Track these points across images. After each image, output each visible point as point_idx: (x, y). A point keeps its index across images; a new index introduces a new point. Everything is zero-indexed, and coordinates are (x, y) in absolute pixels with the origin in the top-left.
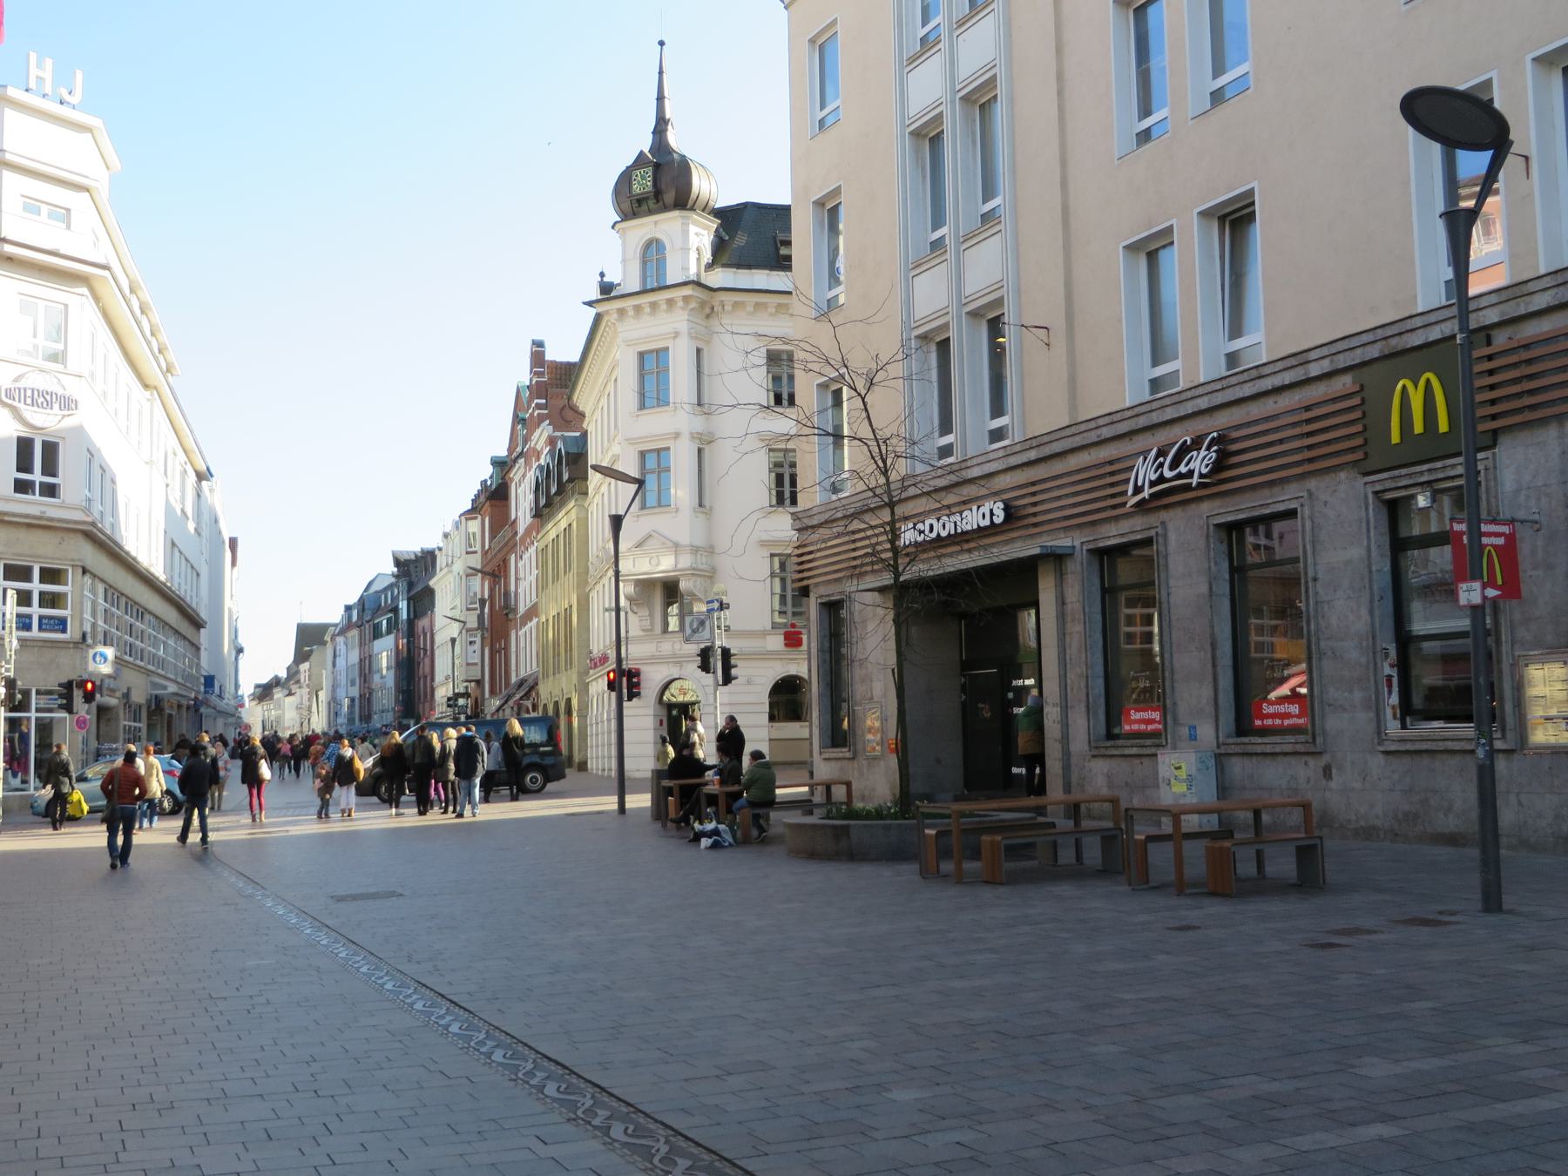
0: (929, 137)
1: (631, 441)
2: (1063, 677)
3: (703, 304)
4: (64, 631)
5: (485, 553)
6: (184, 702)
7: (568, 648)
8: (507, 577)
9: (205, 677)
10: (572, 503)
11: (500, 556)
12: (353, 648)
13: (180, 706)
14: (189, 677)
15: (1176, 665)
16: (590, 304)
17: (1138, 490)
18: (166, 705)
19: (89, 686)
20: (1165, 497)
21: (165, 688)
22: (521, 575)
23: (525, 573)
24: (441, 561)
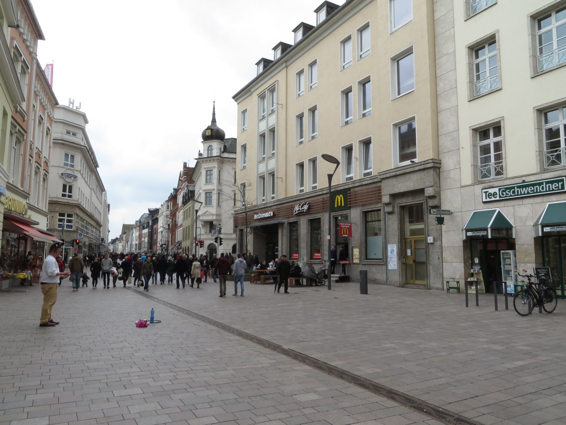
0: (263, 136)
1: (204, 190)
2: (282, 247)
3: (221, 161)
4: (72, 228)
5: (171, 211)
6: (97, 245)
7: (189, 235)
8: (176, 217)
9: (102, 239)
10: (191, 202)
11: (174, 212)
12: (137, 232)
13: (96, 245)
14: (97, 239)
15: (301, 246)
16: (196, 159)
17: (295, 212)
18: (92, 245)
19: (78, 241)
20: (300, 214)
21: (92, 241)
22: (179, 217)
23: (180, 216)
24: (160, 212)
